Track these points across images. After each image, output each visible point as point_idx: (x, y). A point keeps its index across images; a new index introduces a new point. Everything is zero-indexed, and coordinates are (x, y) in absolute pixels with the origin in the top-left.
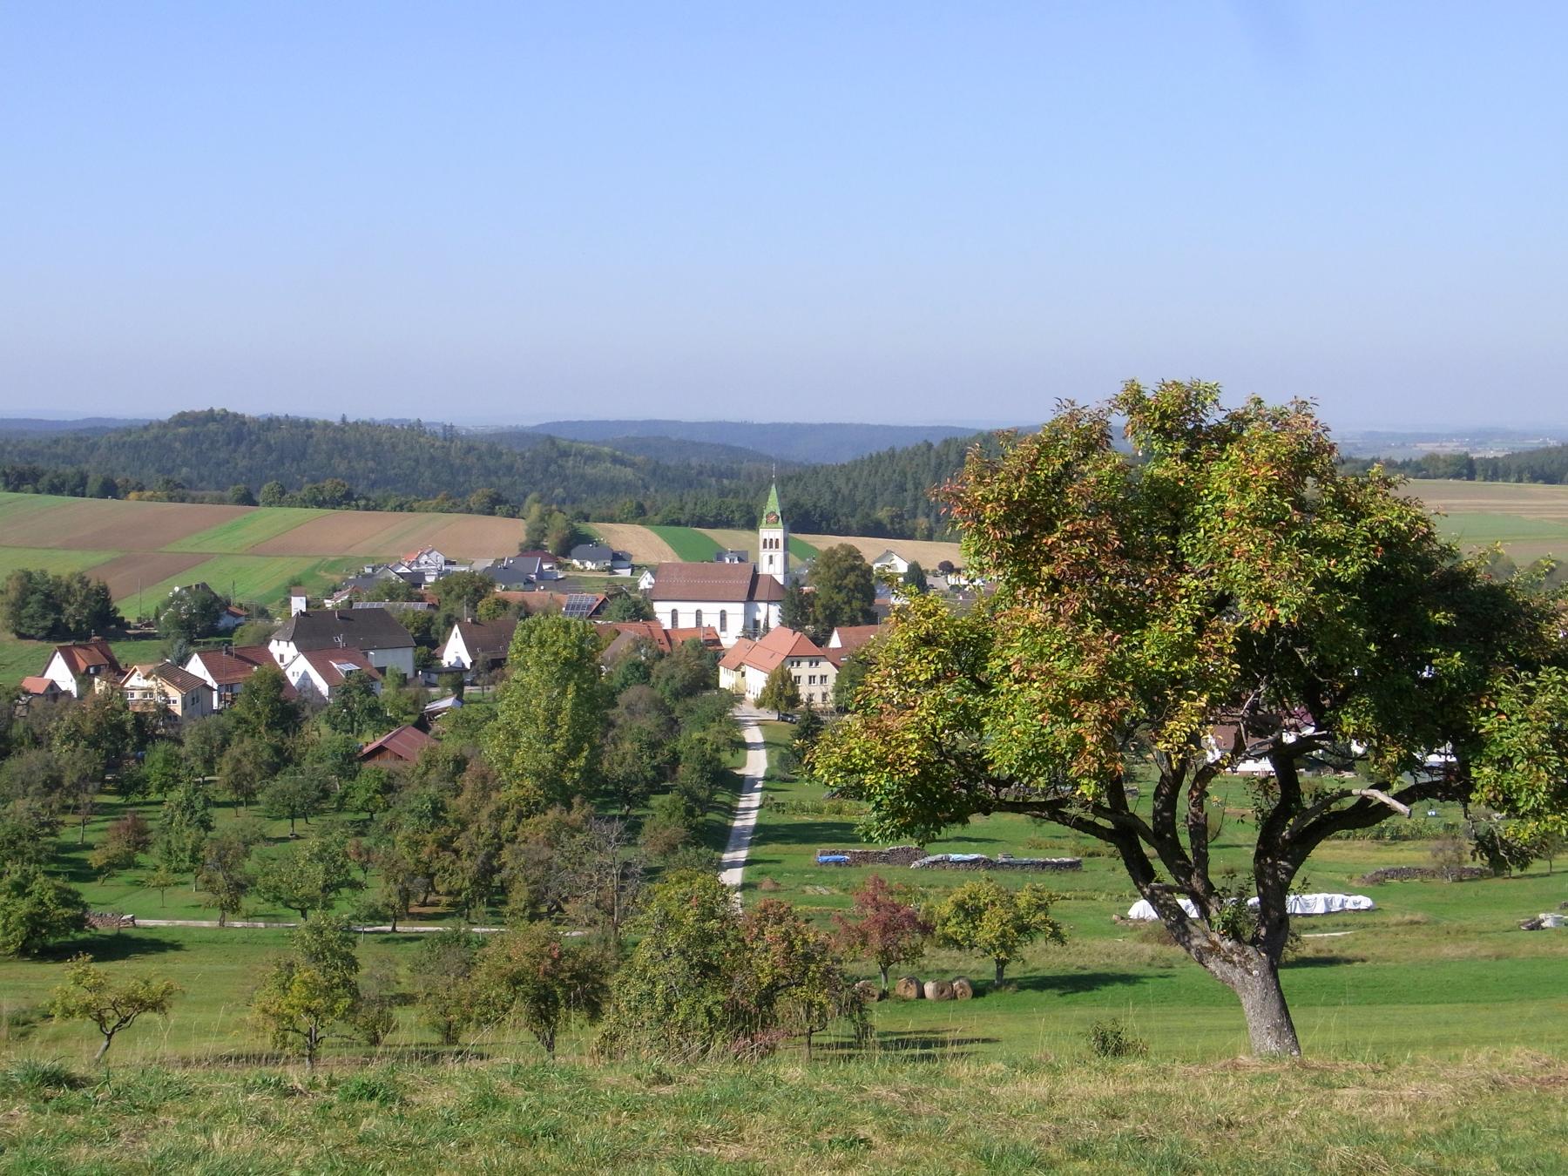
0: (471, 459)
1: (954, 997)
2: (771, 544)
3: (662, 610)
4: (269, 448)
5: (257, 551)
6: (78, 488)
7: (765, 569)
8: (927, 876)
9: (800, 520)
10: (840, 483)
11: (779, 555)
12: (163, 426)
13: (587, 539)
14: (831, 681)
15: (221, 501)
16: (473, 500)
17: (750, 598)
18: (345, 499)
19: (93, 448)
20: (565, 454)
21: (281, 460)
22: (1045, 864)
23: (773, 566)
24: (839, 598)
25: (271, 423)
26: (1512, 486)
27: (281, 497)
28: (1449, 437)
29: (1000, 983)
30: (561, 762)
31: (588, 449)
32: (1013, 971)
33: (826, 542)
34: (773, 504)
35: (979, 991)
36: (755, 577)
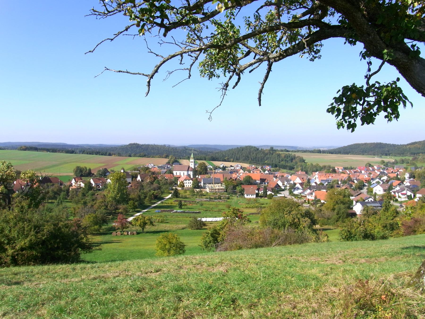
0: (172, 150)
1: (133, 234)
2: (192, 162)
3: (174, 172)
4: (142, 149)
5: (127, 164)
6: (105, 155)
7: (191, 166)
8: (174, 214)
9: (196, 159)
10: (224, 153)
11: (193, 164)
12: (127, 145)
13: (178, 162)
14: (192, 183)
15: (126, 156)
16: (163, 156)
17: (188, 170)
18: (144, 156)
19: (117, 149)
20: (187, 149)
21: (144, 150)
22: (194, 212)
23: (192, 166)
24: (201, 170)
25: (143, 145)
26: (326, 154)
27: (135, 156)
28: (325, 147)
29: (143, 232)
30: (116, 196)
31: (190, 149)
32: (145, 230)
33: (199, 162)
34: (192, 156)
35: (138, 233)
36: (189, 167)
